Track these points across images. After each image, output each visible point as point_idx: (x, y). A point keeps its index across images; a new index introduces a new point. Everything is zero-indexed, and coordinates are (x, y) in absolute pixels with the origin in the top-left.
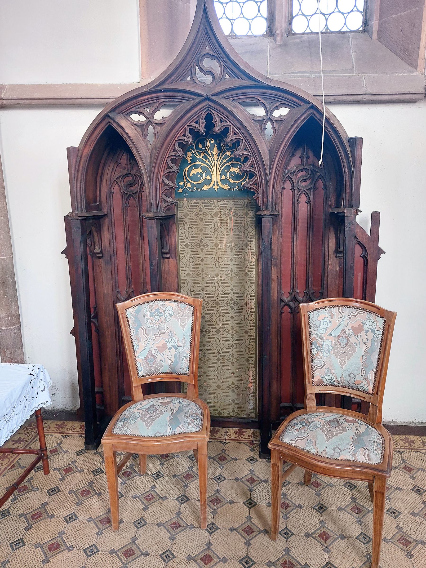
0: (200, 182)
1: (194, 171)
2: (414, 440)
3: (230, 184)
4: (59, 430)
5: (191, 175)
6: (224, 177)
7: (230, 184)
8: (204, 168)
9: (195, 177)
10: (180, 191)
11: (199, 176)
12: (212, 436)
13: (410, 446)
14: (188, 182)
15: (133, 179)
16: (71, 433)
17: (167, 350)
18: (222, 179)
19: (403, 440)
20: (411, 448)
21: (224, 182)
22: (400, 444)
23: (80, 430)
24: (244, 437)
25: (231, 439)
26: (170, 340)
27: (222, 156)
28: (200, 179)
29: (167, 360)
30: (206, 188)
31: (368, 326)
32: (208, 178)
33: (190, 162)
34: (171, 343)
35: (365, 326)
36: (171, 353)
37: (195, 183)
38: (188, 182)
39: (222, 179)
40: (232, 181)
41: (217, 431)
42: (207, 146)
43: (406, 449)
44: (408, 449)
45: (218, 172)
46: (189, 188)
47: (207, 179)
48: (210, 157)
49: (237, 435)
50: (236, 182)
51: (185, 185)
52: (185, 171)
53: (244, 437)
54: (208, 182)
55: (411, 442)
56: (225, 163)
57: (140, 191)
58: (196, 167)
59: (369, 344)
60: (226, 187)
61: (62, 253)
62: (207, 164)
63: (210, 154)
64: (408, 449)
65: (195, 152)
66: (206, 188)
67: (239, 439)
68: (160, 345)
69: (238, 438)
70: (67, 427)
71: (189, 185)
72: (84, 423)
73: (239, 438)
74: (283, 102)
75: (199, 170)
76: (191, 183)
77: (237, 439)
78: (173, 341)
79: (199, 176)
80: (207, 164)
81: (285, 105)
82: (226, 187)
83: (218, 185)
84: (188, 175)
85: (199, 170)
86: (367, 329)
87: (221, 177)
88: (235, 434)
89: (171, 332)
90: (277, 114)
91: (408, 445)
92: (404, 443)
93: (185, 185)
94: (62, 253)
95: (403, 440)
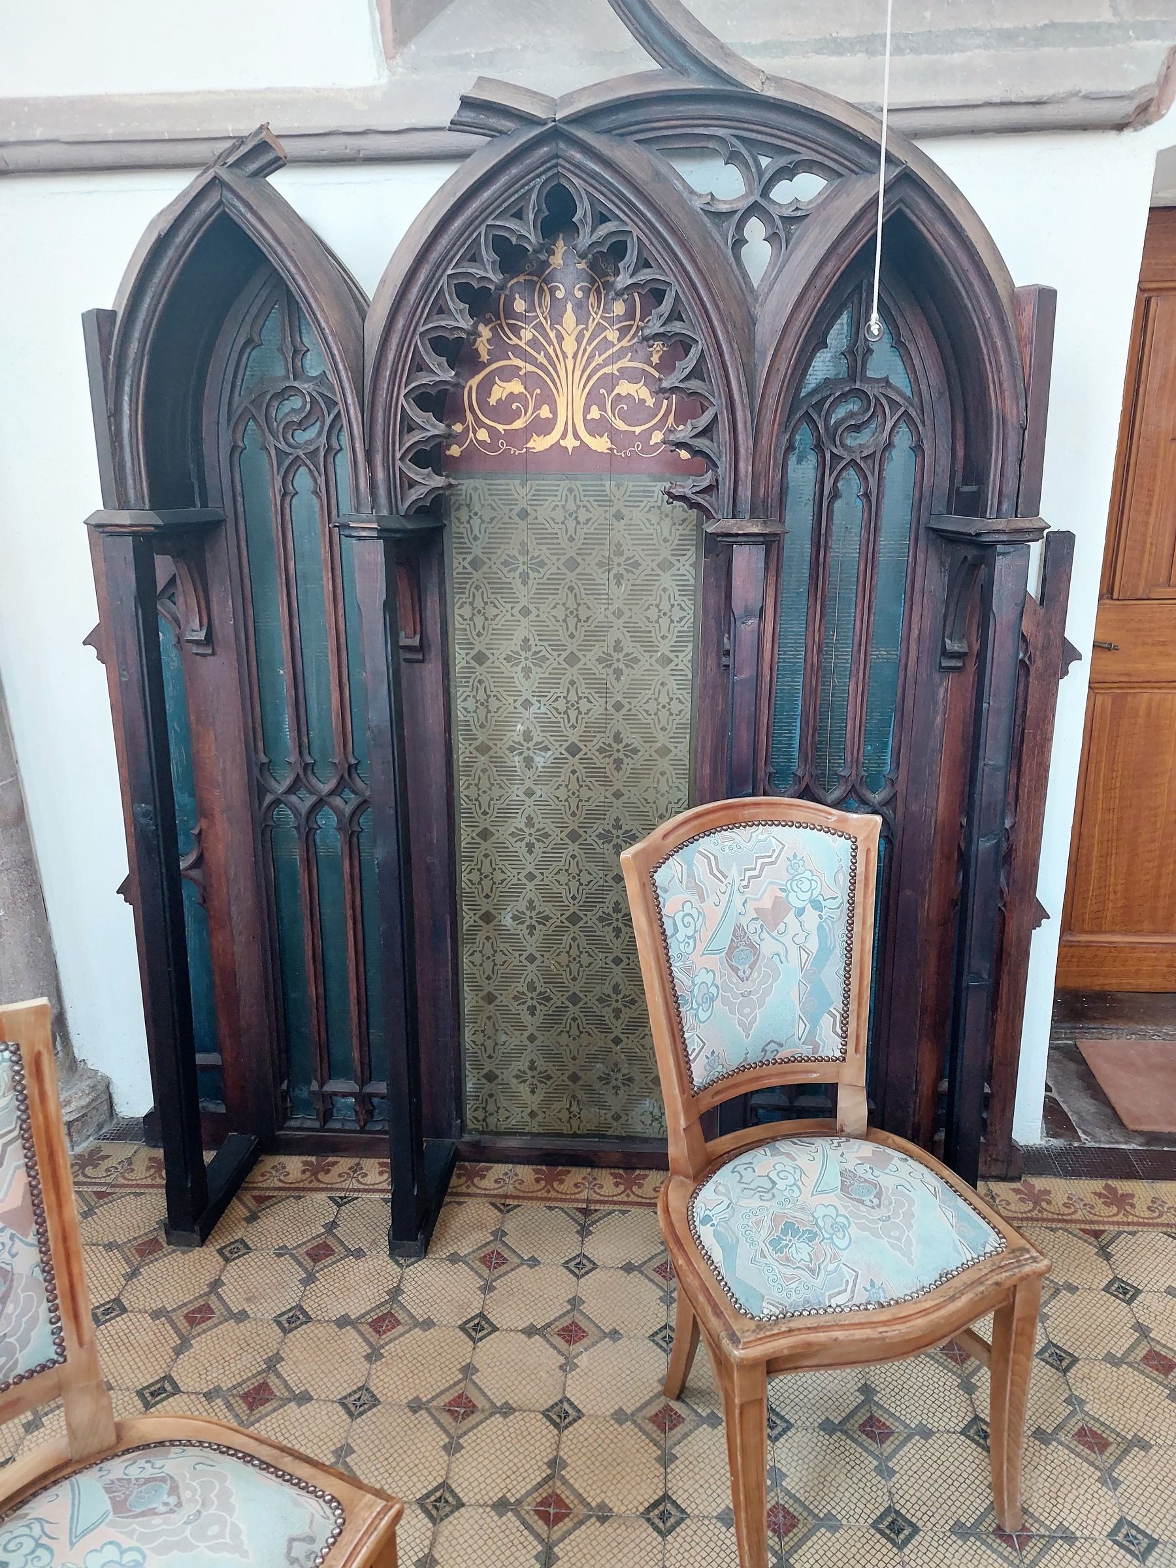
0: (518, 424)
1: (499, 391)
2: (1132, 1196)
3: (613, 434)
4: (85, 1176)
5: (493, 401)
6: (595, 413)
7: (613, 434)
8: (526, 379)
9: (504, 412)
10: (455, 451)
11: (514, 407)
12: (549, 1191)
13: (1121, 1215)
14: (481, 425)
15: (304, 406)
16: (359, 1191)
17: (790, 918)
18: (589, 417)
19: (1100, 1195)
20: (1125, 1219)
21: (595, 428)
22: (1008, 1204)
23: (304, 1177)
24: (561, 1188)
25: (640, 1200)
26: (794, 883)
27: (589, 343)
28: (517, 415)
29: (794, 951)
30: (539, 444)
31: (800, 894)
32: (545, 412)
33: (485, 357)
34: (800, 894)
35: (792, 898)
36: (806, 926)
37: (501, 428)
38: (481, 425)
39: (589, 417)
40: (620, 425)
41: (481, 1170)
42: (540, 304)
43: (1027, 1219)
44: (1032, 1219)
45: (577, 392)
46: (482, 443)
47: (543, 416)
48: (550, 343)
49: (622, 1188)
50: (632, 429)
51: (471, 435)
52: (471, 388)
53: (561, 1188)
54: (543, 427)
55: (1121, 1201)
56: (600, 367)
57: (329, 448)
58: (510, 374)
59: (813, 945)
60: (600, 444)
61: (85, 643)
62: (541, 366)
63: (552, 335)
64: (1032, 1219)
65: (501, 326)
66: (539, 444)
67: (625, 1199)
68: (767, 904)
69: (624, 1198)
70: (106, 1164)
71: (483, 435)
72: (160, 1153)
73: (628, 1196)
74: (807, 155)
75: (516, 387)
76: (488, 428)
77: (619, 1198)
78: (805, 886)
79: (514, 407)
80: (541, 366)
81: (810, 166)
82: (600, 444)
83: (576, 436)
84: (483, 404)
85: (516, 387)
86: (801, 905)
87: (586, 410)
88: (617, 1185)
89: (795, 856)
90: (784, 193)
91: (1115, 1210)
92: (1021, 1200)
93: (471, 435)
94: (85, 643)
95: (1100, 1195)
